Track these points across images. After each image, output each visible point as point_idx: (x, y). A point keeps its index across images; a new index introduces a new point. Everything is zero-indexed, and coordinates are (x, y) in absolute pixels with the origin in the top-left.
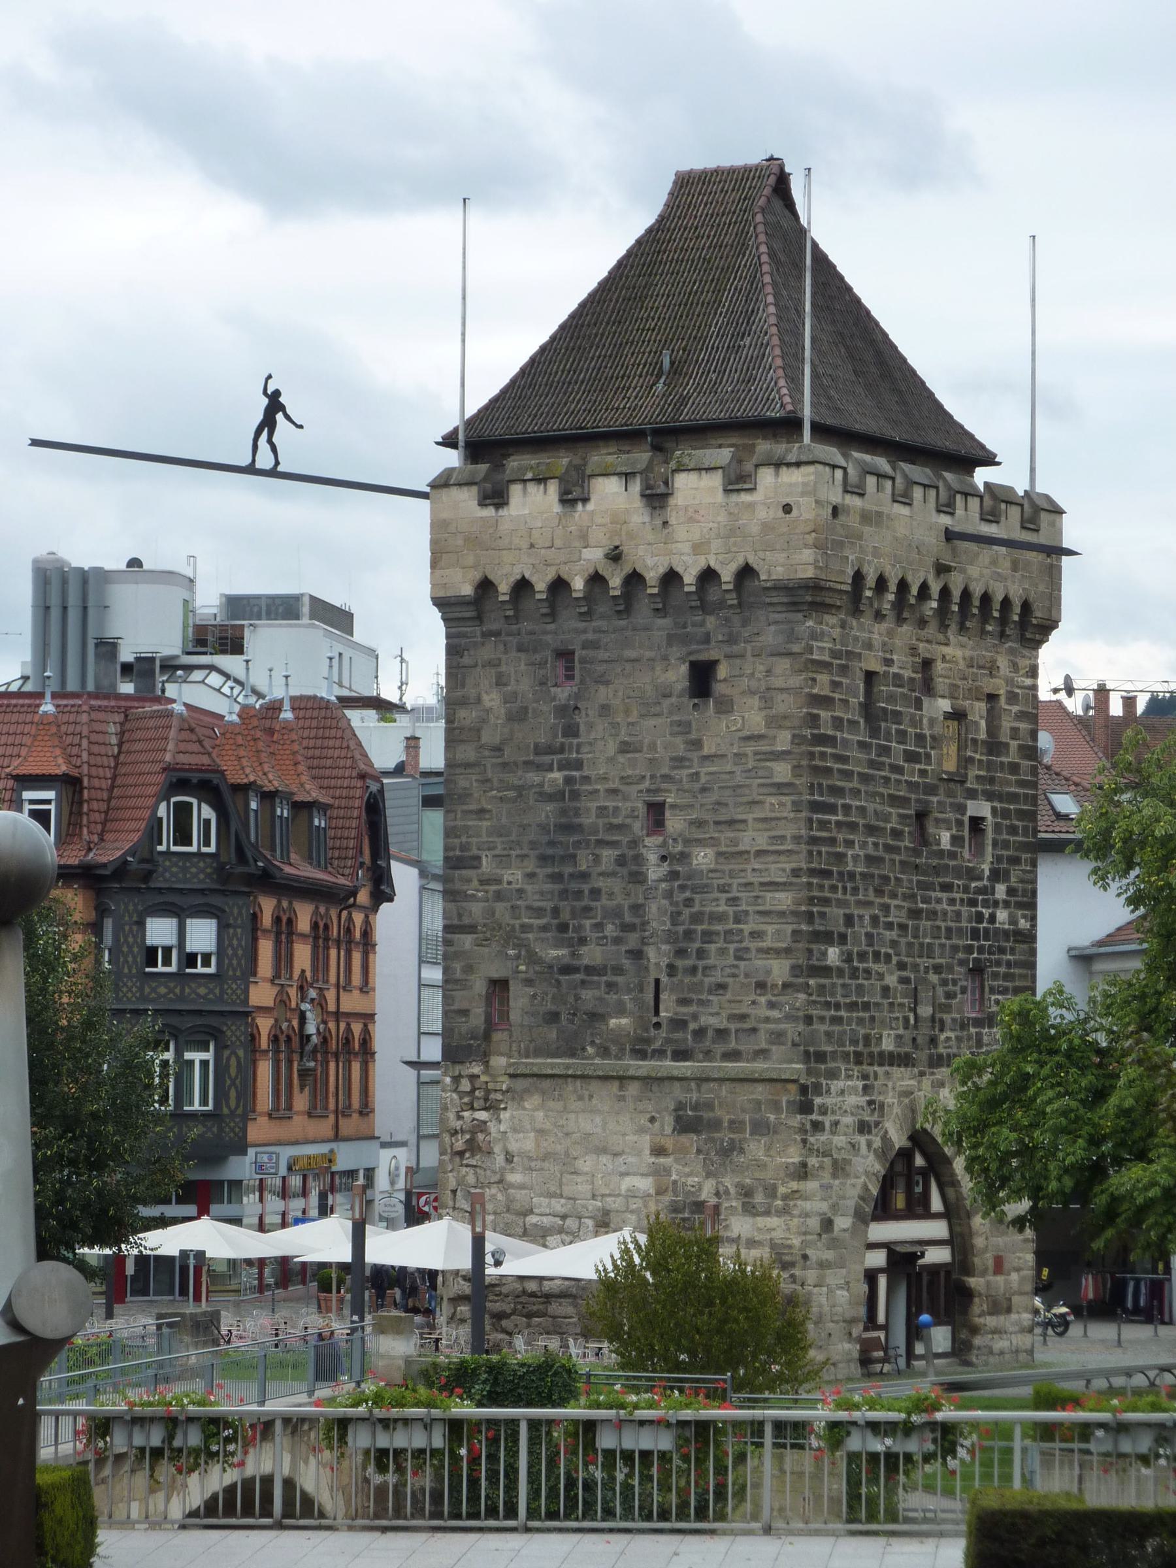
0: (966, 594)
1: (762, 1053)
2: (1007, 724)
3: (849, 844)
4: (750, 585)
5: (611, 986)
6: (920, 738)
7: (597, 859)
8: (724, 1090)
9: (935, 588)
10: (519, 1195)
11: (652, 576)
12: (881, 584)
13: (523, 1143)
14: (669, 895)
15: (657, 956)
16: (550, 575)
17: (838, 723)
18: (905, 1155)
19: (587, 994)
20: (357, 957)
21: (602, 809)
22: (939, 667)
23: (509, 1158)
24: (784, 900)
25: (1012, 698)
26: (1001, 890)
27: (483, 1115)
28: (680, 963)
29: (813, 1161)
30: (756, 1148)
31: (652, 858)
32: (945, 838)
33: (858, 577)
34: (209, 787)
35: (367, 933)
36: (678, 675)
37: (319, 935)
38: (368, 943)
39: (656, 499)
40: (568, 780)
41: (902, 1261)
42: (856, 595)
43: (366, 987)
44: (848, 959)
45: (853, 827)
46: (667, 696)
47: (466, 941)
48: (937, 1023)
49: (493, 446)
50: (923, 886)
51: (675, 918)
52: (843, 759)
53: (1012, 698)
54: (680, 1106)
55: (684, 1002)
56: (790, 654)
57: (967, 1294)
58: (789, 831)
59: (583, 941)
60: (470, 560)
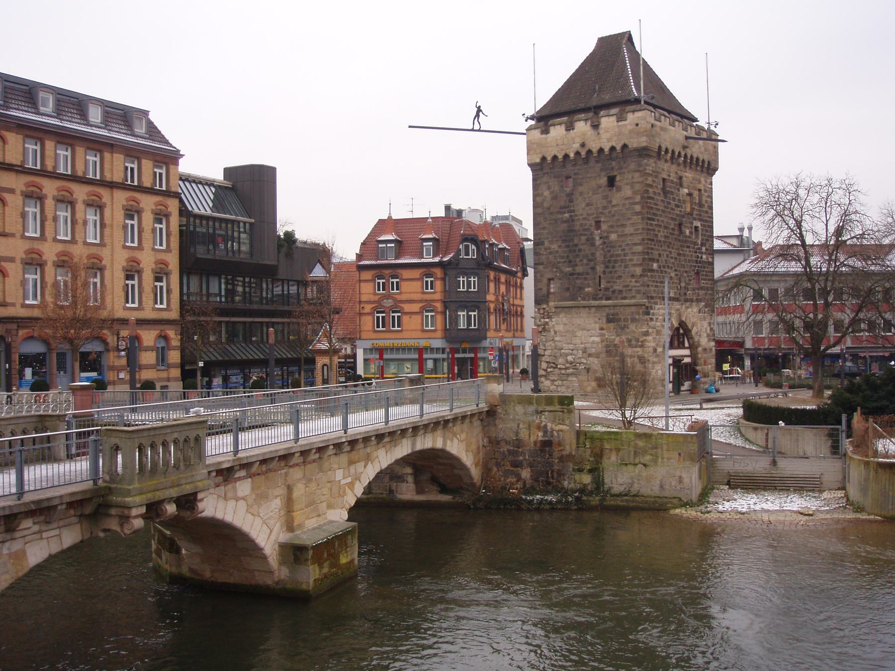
0: (692, 157)
1: (634, 297)
2: (704, 199)
3: (659, 231)
4: (626, 150)
5: (586, 279)
6: (679, 200)
7: (580, 239)
8: (622, 308)
9: (683, 154)
10: (559, 344)
11: (595, 150)
12: (667, 151)
13: (559, 328)
14: (603, 249)
15: (600, 269)
16: (563, 153)
17: (655, 193)
18: (677, 329)
19: (578, 281)
20: (518, 291)
21: (581, 225)
22: (684, 179)
23: (555, 332)
24: (639, 248)
25: (705, 191)
26: (704, 249)
27: (547, 320)
28: (607, 270)
29: (650, 330)
30: (632, 327)
31: (597, 238)
32: (687, 232)
33: (660, 147)
34: (474, 240)
35: (521, 284)
36: (604, 181)
37: (507, 283)
38: (521, 287)
39: (596, 127)
40: (571, 216)
41: (677, 362)
42: (659, 153)
43: (521, 298)
44: (660, 267)
45: (660, 226)
46: (600, 187)
47: (541, 267)
48: (686, 289)
49: (544, 119)
50: (681, 246)
51: (605, 256)
52: (656, 205)
53: (705, 191)
54: (608, 315)
55: (609, 282)
56: (639, 171)
57: (696, 372)
58: (640, 227)
59: (576, 265)
60: (538, 151)
